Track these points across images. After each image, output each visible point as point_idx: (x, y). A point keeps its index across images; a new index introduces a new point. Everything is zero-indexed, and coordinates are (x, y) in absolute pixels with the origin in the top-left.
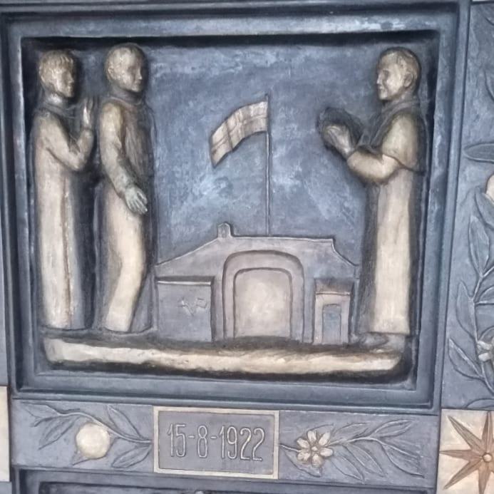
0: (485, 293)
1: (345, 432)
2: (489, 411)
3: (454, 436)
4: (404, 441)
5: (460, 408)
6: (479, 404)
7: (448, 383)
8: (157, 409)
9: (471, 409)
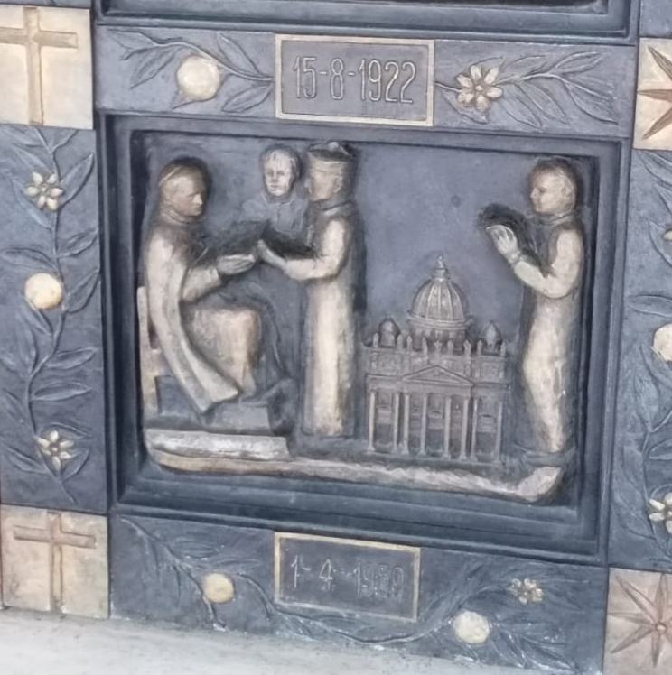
1: (518, 67)
3: (656, 72)
4: (592, 79)
8: (279, 38)
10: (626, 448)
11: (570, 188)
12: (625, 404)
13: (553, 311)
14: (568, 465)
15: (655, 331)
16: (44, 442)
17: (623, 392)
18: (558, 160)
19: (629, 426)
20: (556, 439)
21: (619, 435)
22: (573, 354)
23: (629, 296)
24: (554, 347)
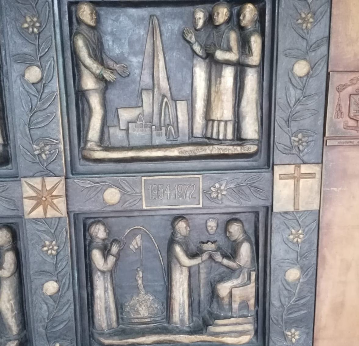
0: (33, 123)
1: (231, 183)
2: (43, 177)
3: (28, 190)
4: (6, 194)
5: (31, 177)
6: (38, 174)
7: (23, 165)
8: (144, 178)
9: (35, 177)
10: (39, 329)
11: (9, 235)
12: (37, 313)
13: (7, 282)
14: (22, 339)
15: (43, 285)
16: (289, 333)
17: (35, 309)
18: (4, 225)
19: (39, 321)
20: (15, 329)
21: (36, 325)
22: (18, 297)
23: (33, 273)
24: (9, 296)
